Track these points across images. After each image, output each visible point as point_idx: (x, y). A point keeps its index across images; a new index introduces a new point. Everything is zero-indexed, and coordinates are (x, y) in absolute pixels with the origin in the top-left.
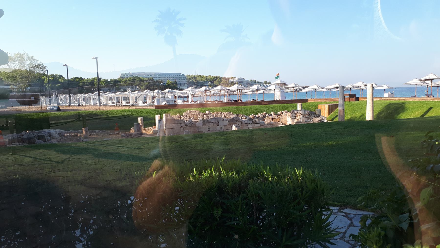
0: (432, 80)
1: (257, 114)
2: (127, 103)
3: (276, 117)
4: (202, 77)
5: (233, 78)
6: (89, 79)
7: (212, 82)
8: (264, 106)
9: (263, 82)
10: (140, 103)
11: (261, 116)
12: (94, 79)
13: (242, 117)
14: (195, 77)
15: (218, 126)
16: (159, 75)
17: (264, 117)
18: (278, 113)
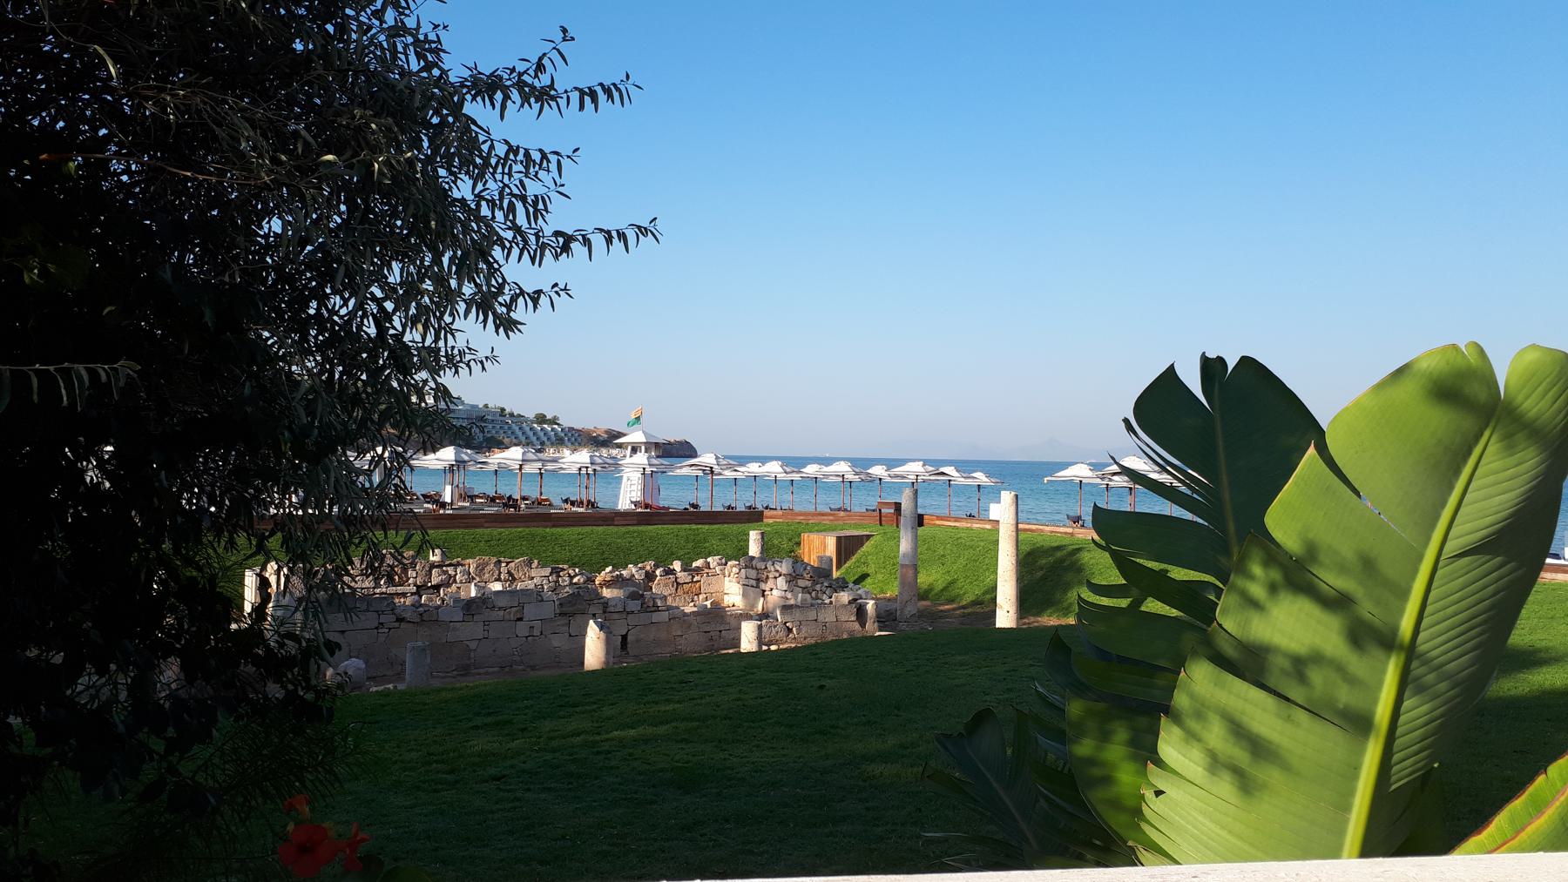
1: (625, 567)
8: (623, 529)
9: (531, 415)
11: (640, 576)
13: (571, 577)
15: (520, 619)
17: (650, 577)
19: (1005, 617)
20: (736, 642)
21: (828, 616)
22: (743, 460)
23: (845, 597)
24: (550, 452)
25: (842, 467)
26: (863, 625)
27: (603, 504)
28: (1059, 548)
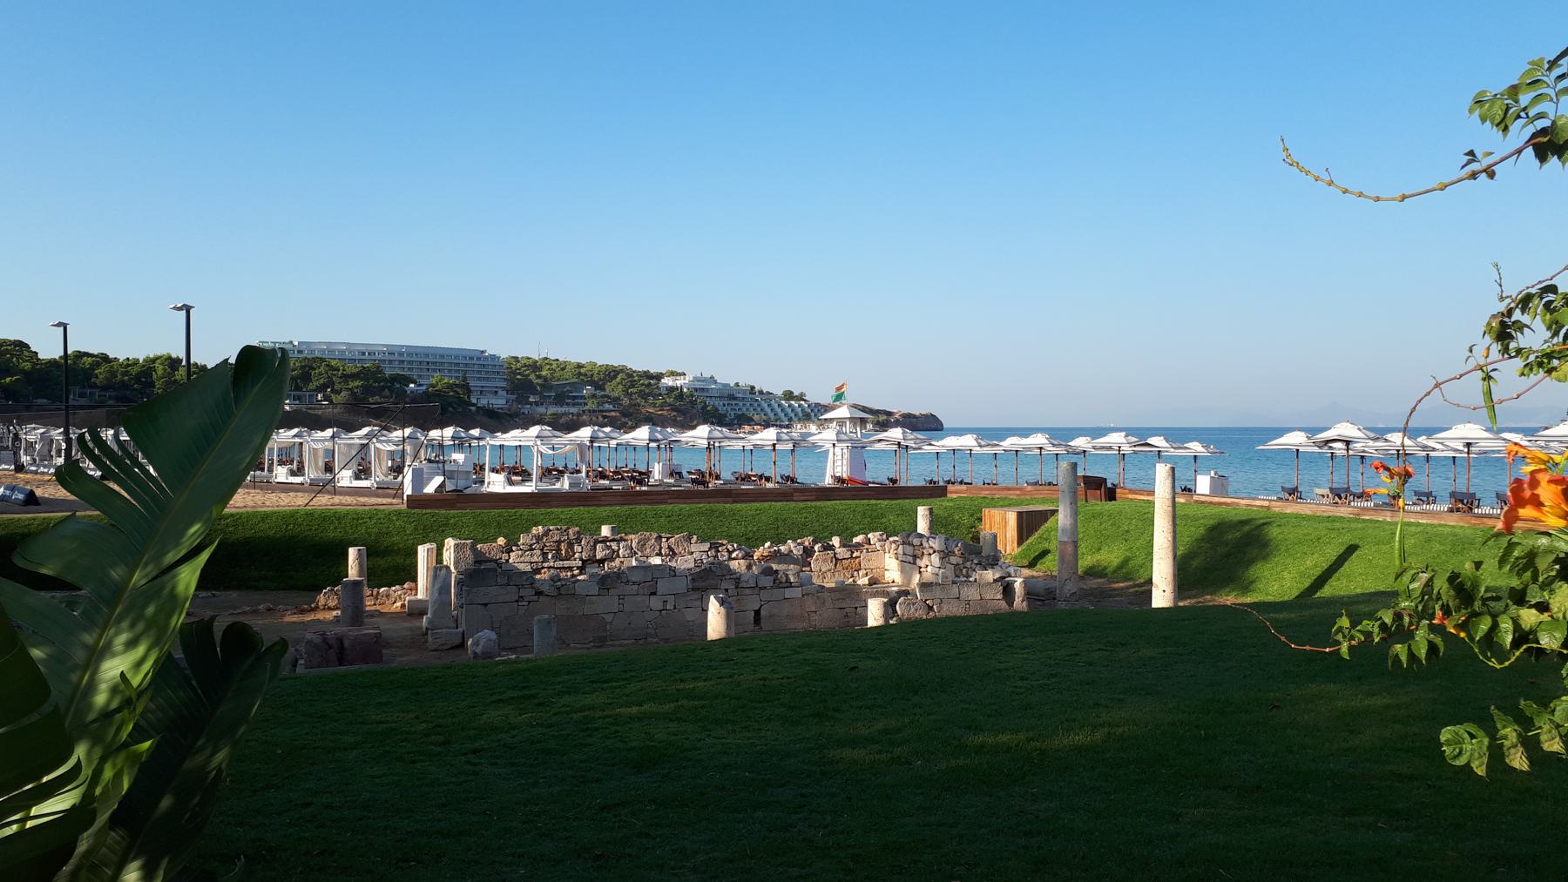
0: (1348, 443)
2: (293, 473)
3: (848, 555)
4: (563, 366)
5: (672, 374)
6: (136, 362)
7: (598, 386)
8: (802, 505)
9: (779, 392)
10: (345, 478)
12: (154, 360)
13: (730, 553)
14: (535, 366)
15: (654, 594)
16: (401, 354)
17: (808, 552)
18: (855, 540)
19: (1162, 598)
20: (35, 646)
21: (971, 593)
22: (1003, 433)
23: (990, 575)
24: (798, 429)
25: (1039, 439)
26: (1010, 603)
27: (805, 477)
28: (1243, 523)
